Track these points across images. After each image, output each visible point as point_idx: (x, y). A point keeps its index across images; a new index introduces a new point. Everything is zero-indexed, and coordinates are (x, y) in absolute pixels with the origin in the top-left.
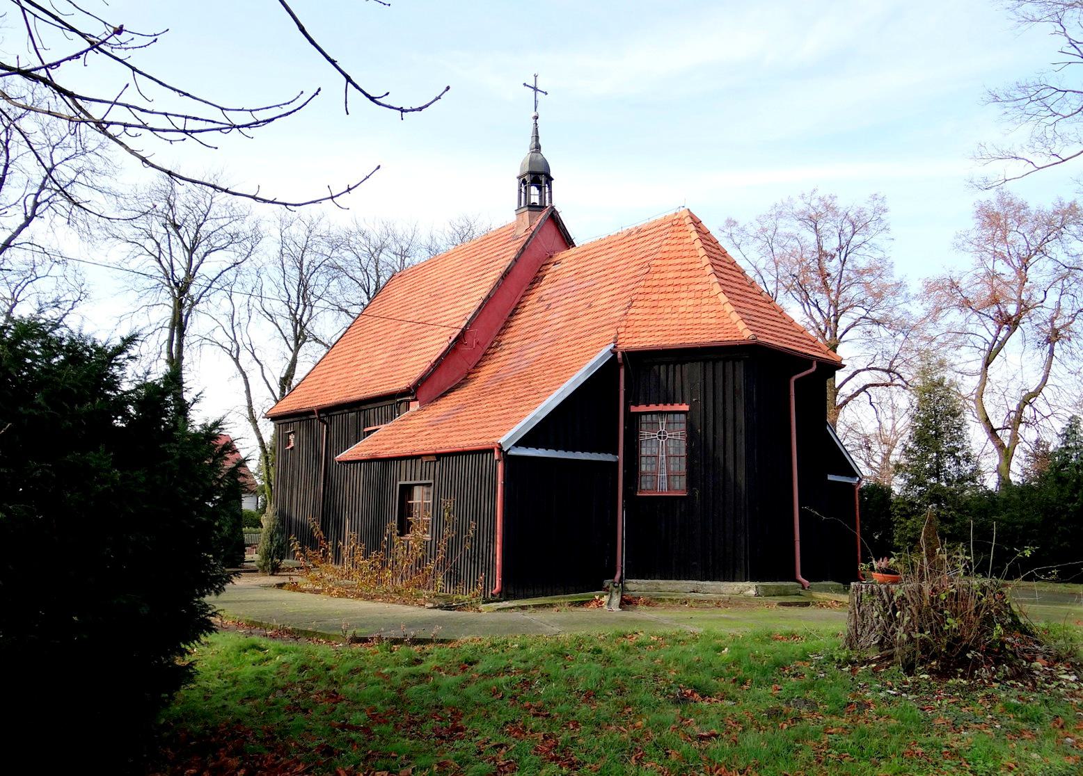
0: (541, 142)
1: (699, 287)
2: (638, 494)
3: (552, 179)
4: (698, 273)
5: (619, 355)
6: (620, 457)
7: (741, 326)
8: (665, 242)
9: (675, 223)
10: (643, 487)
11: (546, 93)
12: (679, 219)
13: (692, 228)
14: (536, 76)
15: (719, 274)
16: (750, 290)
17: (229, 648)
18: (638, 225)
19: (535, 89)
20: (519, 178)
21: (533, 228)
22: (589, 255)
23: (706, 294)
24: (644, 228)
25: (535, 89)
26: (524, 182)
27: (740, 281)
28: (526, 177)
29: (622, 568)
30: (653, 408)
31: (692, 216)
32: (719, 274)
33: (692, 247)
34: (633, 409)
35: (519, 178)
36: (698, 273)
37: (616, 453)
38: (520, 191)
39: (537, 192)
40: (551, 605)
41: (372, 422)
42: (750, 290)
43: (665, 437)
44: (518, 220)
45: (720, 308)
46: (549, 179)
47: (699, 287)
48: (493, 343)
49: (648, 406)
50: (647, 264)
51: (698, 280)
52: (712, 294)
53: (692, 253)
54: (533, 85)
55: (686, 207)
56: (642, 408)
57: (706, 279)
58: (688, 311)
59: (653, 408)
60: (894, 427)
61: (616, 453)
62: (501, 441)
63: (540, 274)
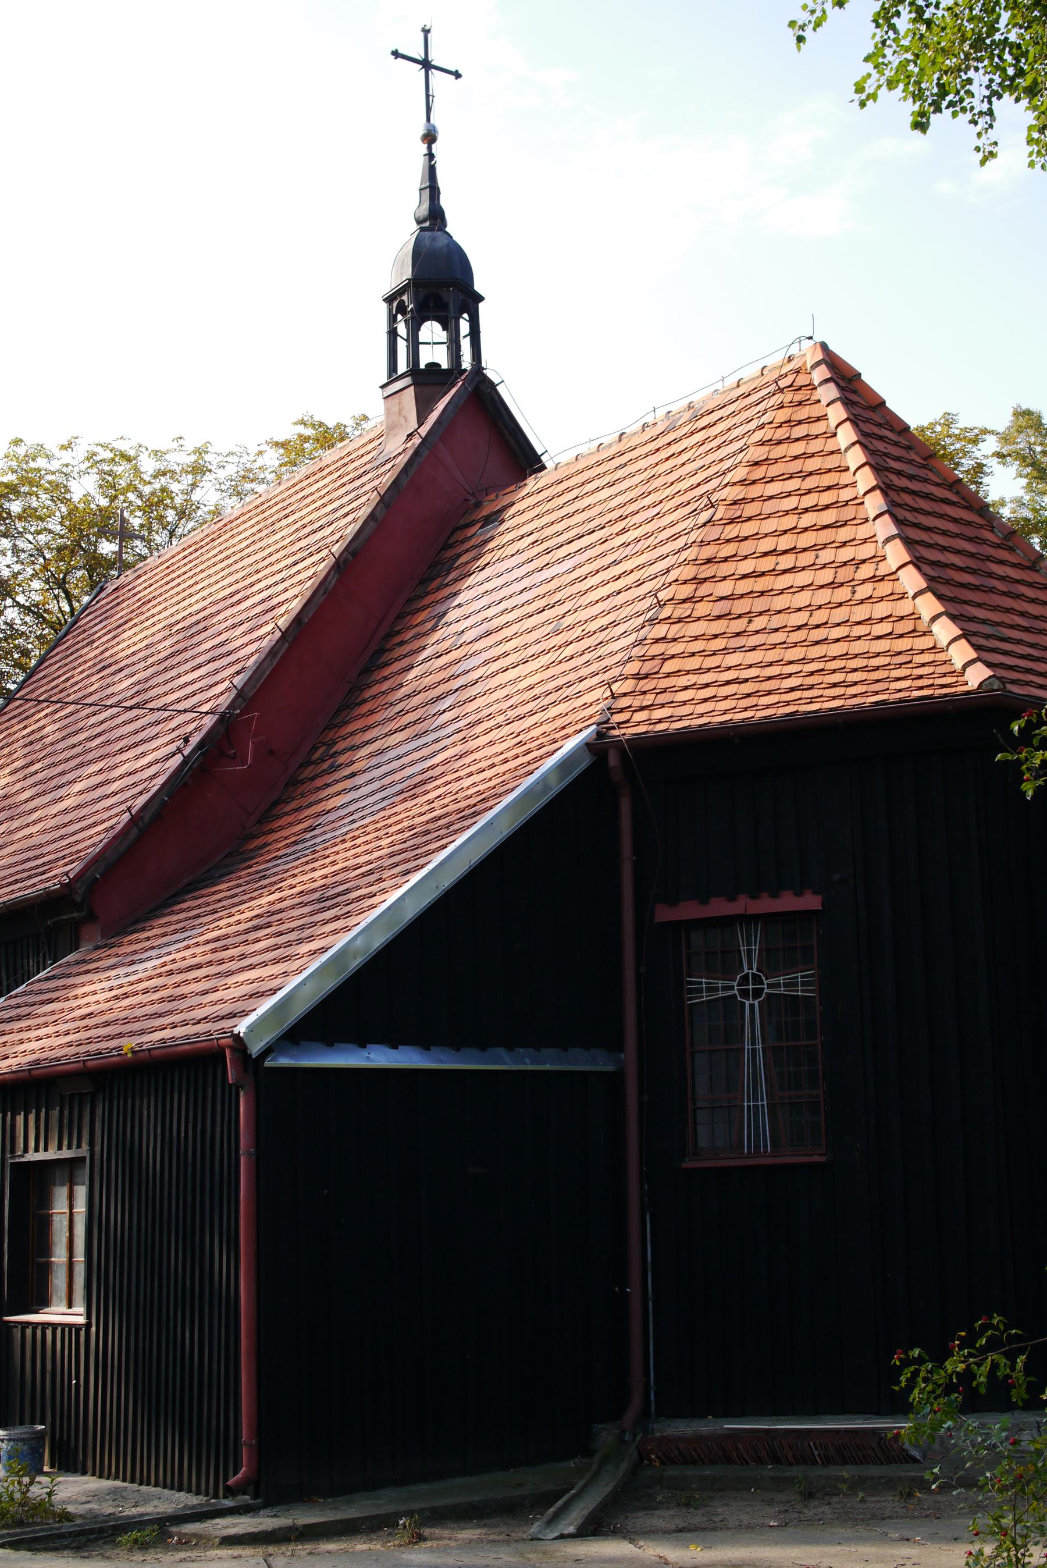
0: (444, 202)
1: (845, 554)
2: (687, 1164)
3: (480, 298)
4: (848, 513)
5: (613, 760)
6: (629, 1056)
7: (961, 653)
8: (758, 436)
9: (783, 383)
10: (703, 1142)
11: (457, 75)
12: (798, 372)
13: (830, 392)
14: (426, 32)
15: (902, 514)
16: (1004, 555)
17: (125, 1552)
18: (695, 398)
19: (426, 65)
20: (389, 300)
21: (424, 430)
22: (569, 490)
23: (866, 571)
24: (710, 406)
25: (426, 65)
26: (402, 309)
27: (970, 532)
28: (405, 298)
29: (647, 1384)
30: (719, 907)
31: (831, 360)
32: (902, 514)
33: (831, 445)
34: (664, 914)
35: (389, 300)
36: (848, 513)
37: (616, 1045)
38: (393, 334)
39: (442, 335)
40: (240, 1556)
41: (5, 991)
42: (1004, 555)
43: (744, 993)
44: (388, 412)
45: (904, 608)
46: (471, 301)
47: (845, 554)
48: (315, 748)
49: (704, 902)
50: (705, 500)
51: (844, 534)
52: (883, 570)
53: (832, 462)
54: (419, 54)
55: (818, 339)
56: (689, 910)
57: (863, 532)
58: (814, 621)
59: (719, 907)
60: (58, 602)
61: (616, 1045)
62: (242, 1027)
63: (449, 554)
